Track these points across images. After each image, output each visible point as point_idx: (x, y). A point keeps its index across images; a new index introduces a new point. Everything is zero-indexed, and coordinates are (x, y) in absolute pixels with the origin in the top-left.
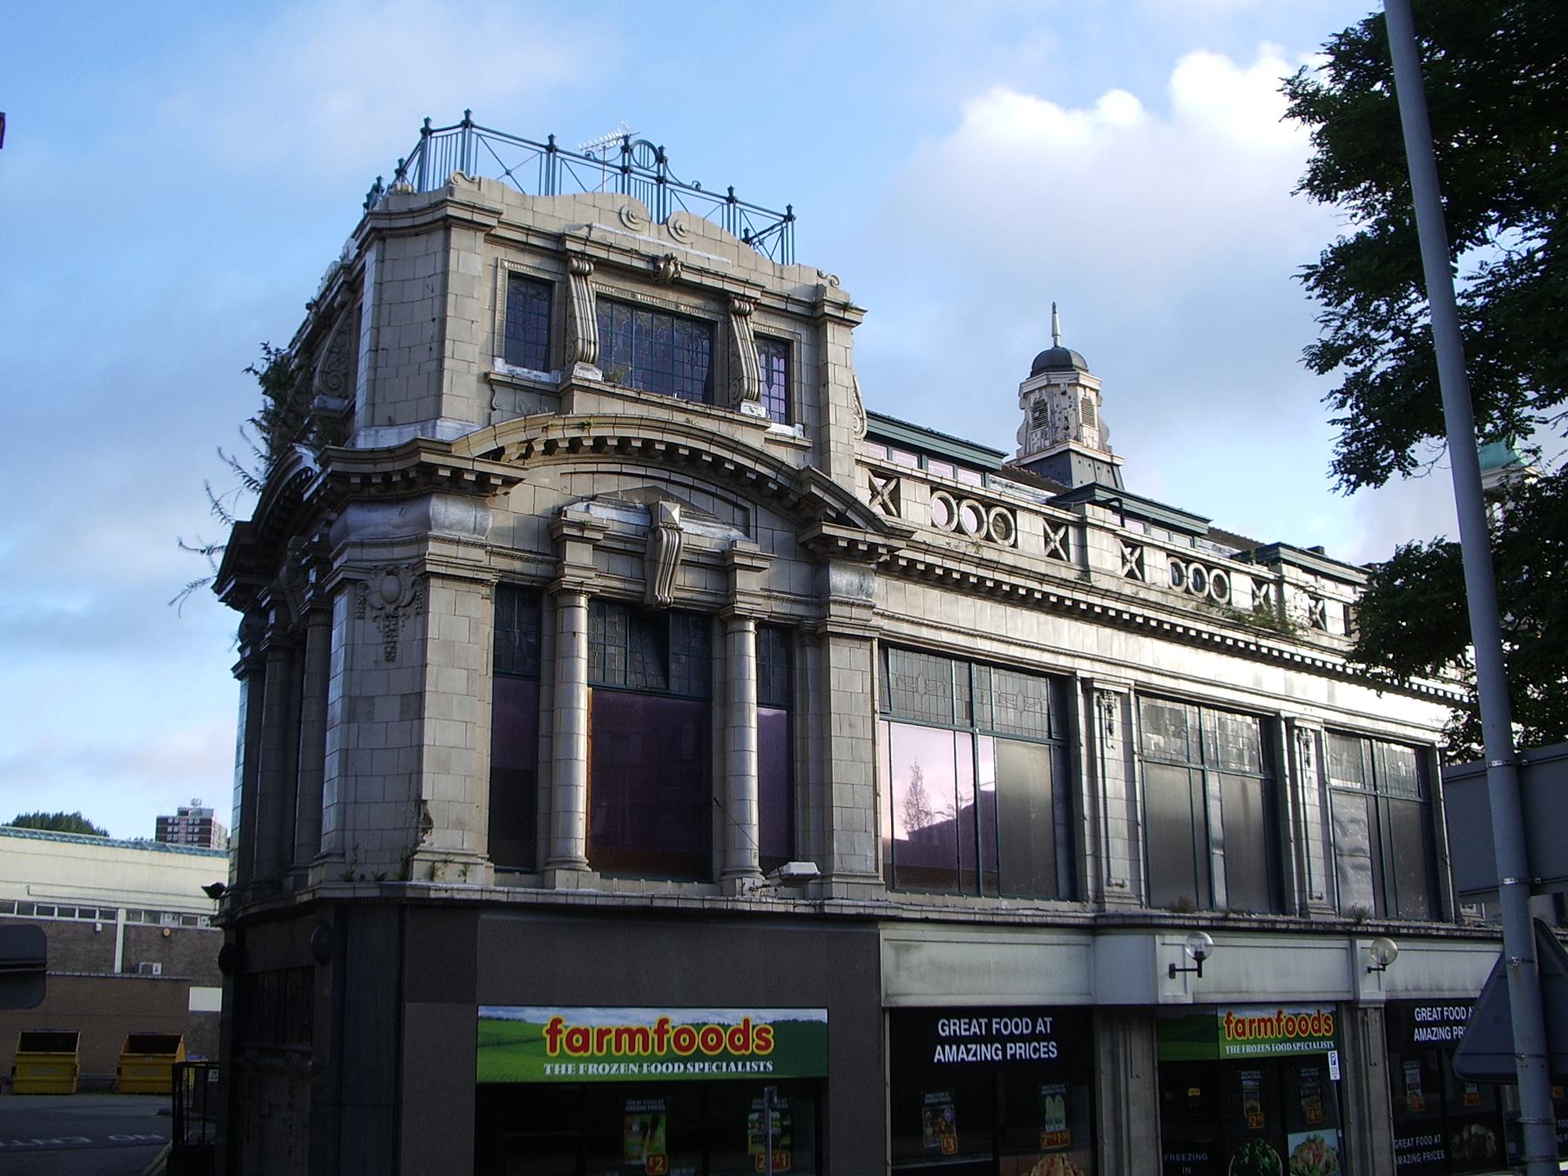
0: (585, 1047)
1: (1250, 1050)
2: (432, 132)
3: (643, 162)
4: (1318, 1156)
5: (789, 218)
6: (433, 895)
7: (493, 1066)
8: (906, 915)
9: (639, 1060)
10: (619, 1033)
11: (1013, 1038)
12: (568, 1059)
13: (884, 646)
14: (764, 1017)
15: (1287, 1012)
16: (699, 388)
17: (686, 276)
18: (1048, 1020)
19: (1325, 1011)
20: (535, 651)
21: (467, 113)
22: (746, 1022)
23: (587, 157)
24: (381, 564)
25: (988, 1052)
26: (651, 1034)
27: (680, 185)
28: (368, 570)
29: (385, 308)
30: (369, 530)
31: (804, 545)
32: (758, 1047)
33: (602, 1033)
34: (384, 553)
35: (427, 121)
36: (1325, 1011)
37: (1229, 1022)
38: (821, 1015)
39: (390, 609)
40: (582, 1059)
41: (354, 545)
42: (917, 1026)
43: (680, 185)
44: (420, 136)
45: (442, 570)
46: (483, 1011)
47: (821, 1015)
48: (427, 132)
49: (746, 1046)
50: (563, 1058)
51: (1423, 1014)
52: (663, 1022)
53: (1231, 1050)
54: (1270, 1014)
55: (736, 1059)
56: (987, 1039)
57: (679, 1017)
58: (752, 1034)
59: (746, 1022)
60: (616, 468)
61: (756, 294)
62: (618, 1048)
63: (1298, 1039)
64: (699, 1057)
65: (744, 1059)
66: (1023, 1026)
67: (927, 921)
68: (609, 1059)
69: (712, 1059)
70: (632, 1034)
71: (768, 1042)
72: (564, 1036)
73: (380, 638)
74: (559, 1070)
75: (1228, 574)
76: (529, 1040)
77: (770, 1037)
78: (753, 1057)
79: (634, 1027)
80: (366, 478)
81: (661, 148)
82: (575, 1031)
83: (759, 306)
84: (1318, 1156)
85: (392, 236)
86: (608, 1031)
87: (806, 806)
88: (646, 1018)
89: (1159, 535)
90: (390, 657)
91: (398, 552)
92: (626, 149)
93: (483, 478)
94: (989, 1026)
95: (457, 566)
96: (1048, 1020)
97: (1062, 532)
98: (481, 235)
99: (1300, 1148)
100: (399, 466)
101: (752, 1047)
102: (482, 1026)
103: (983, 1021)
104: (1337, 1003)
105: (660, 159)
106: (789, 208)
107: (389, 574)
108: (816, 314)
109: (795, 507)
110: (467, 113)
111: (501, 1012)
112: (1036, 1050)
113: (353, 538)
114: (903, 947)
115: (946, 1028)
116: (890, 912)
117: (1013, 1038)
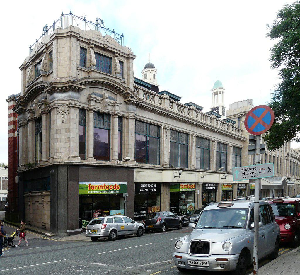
0: (94, 189)
1: (184, 190)
2: (63, 15)
3: (100, 23)
4: (191, 208)
5: (123, 36)
6: (73, 163)
7: (82, 192)
8: (139, 167)
9: (101, 191)
10: (98, 186)
11: (151, 188)
12: (91, 191)
13: (136, 120)
14: (118, 184)
15: (189, 184)
16: (108, 71)
17: (109, 48)
18: (155, 185)
19: (194, 184)
20: (85, 120)
21: (71, 11)
22: (116, 184)
23: (90, 22)
24: (61, 104)
25: (147, 190)
26: (103, 187)
27: (106, 29)
28: (58, 106)
29: (59, 53)
30: (59, 98)
31: (125, 102)
32: (117, 189)
33: (96, 186)
34: (61, 102)
35: (62, 12)
36: (194, 184)
37: (181, 185)
38: (126, 183)
39: (63, 113)
40: (94, 191)
41: (56, 101)
42: (138, 185)
43: (106, 29)
44: (61, 16)
45: (73, 106)
46: (80, 183)
47: (126, 183)
48: (62, 15)
49: (116, 188)
50: (91, 191)
51: (207, 185)
52: (105, 184)
53: (181, 190)
54: (186, 184)
55: (114, 191)
56: (147, 188)
57: (107, 184)
58: (117, 187)
59: (116, 184)
60: (105, 88)
61: (119, 52)
62: (98, 189)
63: (190, 189)
64: (109, 190)
65: (115, 190)
66: (152, 186)
67: (141, 168)
68: (97, 191)
69: (111, 191)
70: (100, 186)
71: (118, 187)
72: (91, 187)
73: (61, 118)
74: (90, 192)
75: (154, 96)
76: (86, 188)
77: (119, 187)
78: (117, 190)
79: (100, 185)
80: (58, 88)
81: (103, 20)
82: (92, 186)
83: (120, 55)
84: (191, 208)
85: (59, 38)
86: (97, 186)
87: (124, 148)
88: (102, 184)
89: (142, 87)
90: (63, 122)
91: (64, 102)
92: (97, 20)
93: (79, 88)
94: (148, 185)
95: (75, 105)
96: (155, 185)
97: (161, 100)
98: (76, 39)
99: (189, 206)
100: (65, 85)
101: (117, 188)
102: (80, 185)
103: (147, 185)
104: (196, 183)
105: (103, 23)
106: (123, 34)
107: (62, 106)
108: (130, 57)
109: (124, 95)
110: (71, 11)
111: (82, 183)
112: (154, 190)
113: (56, 99)
114: (138, 172)
115: (142, 186)
116: (137, 166)
117: (151, 188)
